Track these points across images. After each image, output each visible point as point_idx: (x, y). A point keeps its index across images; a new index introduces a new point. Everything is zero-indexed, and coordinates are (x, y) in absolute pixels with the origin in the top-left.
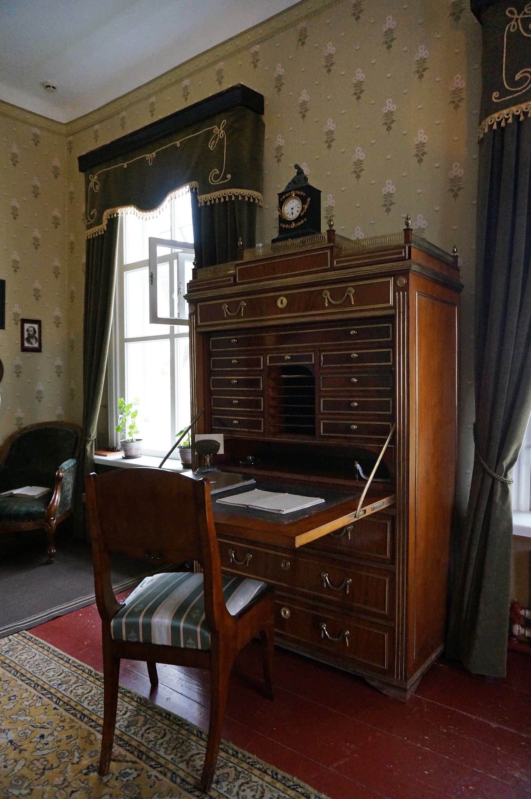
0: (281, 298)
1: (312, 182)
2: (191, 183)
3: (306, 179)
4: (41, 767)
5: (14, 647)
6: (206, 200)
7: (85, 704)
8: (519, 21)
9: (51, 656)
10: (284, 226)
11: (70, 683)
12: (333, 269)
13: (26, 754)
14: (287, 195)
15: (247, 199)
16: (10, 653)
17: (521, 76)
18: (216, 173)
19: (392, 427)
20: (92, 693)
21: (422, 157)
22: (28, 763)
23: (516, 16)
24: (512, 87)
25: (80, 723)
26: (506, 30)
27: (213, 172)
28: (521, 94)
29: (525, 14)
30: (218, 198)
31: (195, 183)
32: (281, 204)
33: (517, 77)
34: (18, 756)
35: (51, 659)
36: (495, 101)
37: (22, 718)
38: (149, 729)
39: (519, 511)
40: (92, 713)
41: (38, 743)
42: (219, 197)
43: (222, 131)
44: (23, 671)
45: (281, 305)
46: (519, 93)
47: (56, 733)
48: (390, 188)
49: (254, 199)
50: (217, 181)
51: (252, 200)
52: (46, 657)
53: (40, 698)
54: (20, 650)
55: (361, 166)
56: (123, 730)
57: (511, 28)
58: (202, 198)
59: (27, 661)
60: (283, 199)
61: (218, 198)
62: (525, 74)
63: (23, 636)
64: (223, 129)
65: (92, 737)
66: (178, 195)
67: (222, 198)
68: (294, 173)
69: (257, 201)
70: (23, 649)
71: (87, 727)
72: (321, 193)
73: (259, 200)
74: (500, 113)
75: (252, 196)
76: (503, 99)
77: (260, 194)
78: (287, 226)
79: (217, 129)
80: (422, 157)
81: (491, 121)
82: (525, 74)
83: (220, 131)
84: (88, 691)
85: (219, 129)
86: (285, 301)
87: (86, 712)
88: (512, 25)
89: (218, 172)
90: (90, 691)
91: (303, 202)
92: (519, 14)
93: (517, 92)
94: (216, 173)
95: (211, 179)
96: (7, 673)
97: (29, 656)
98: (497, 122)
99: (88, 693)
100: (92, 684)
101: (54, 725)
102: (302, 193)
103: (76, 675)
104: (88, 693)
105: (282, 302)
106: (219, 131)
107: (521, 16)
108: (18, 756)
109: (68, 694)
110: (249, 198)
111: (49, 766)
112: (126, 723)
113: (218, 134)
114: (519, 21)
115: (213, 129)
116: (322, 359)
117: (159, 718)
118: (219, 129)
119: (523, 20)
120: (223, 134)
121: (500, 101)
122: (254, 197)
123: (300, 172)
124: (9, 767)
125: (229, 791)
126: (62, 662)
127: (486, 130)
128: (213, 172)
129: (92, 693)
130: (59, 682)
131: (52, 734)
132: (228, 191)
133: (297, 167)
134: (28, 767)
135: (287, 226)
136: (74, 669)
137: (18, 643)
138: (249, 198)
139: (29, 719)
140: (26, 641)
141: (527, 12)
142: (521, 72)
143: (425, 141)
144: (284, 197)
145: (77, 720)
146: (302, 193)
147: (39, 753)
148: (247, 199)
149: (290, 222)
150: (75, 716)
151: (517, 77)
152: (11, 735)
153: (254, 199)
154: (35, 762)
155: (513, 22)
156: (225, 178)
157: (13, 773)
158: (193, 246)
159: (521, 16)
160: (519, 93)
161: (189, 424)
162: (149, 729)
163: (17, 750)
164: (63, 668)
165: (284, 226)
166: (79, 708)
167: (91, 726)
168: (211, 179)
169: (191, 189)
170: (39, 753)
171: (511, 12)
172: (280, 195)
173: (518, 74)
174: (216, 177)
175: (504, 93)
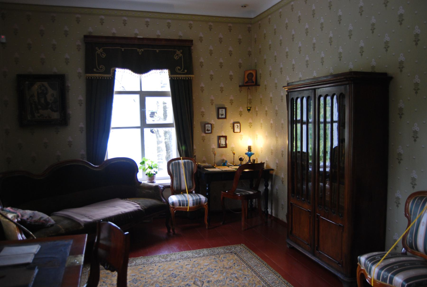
4: (243, 285)
5: (242, 251)
7: (261, 273)
9: (254, 256)
11: (276, 283)
13: (240, 281)
16: (240, 253)
19: (415, 223)
20: (264, 271)
22: (240, 283)
23: (180, 52)
25: (258, 277)
33: (100, 67)
34: (237, 281)
35: (253, 257)
37: (240, 272)
38: (279, 285)
40: (262, 276)
41: (244, 279)
44: (243, 259)
47: (250, 278)
50: (179, 71)
52: (252, 257)
53: (247, 268)
54: (278, 284)
56: (271, 283)
59: (262, 271)
63: (245, 248)
65: (260, 282)
70: (260, 266)
71: (260, 279)
84: (263, 270)
87: (261, 276)
90: (264, 270)
93: (100, 71)
95: (103, 70)
96: (238, 258)
97: (272, 278)
99: (263, 271)
100: (265, 268)
101: (249, 276)
103: (260, 264)
104: (263, 271)
108: (237, 281)
109: (256, 269)
111: (245, 285)
112: (272, 282)
117: (284, 283)
124: (234, 283)
125: (274, 285)
126: (257, 259)
128: (177, 71)
129: (264, 271)
130: (254, 265)
131: (248, 278)
134: (239, 284)
136: (260, 262)
137: (243, 250)
139: (242, 272)
140: (246, 250)
145: (257, 277)
147: (243, 282)
150: (257, 275)
151: (100, 67)
152: (236, 275)
153: (191, 78)
154: (242, 283)
156: (183, 71)
157: (235, 284)
162: (279, 285)
163: (237, 279)
164: (257, 261)
166: (259, 274)
167: (261, 279)
168: (103, 70)
170: (243, 282)
174: (179, 70)
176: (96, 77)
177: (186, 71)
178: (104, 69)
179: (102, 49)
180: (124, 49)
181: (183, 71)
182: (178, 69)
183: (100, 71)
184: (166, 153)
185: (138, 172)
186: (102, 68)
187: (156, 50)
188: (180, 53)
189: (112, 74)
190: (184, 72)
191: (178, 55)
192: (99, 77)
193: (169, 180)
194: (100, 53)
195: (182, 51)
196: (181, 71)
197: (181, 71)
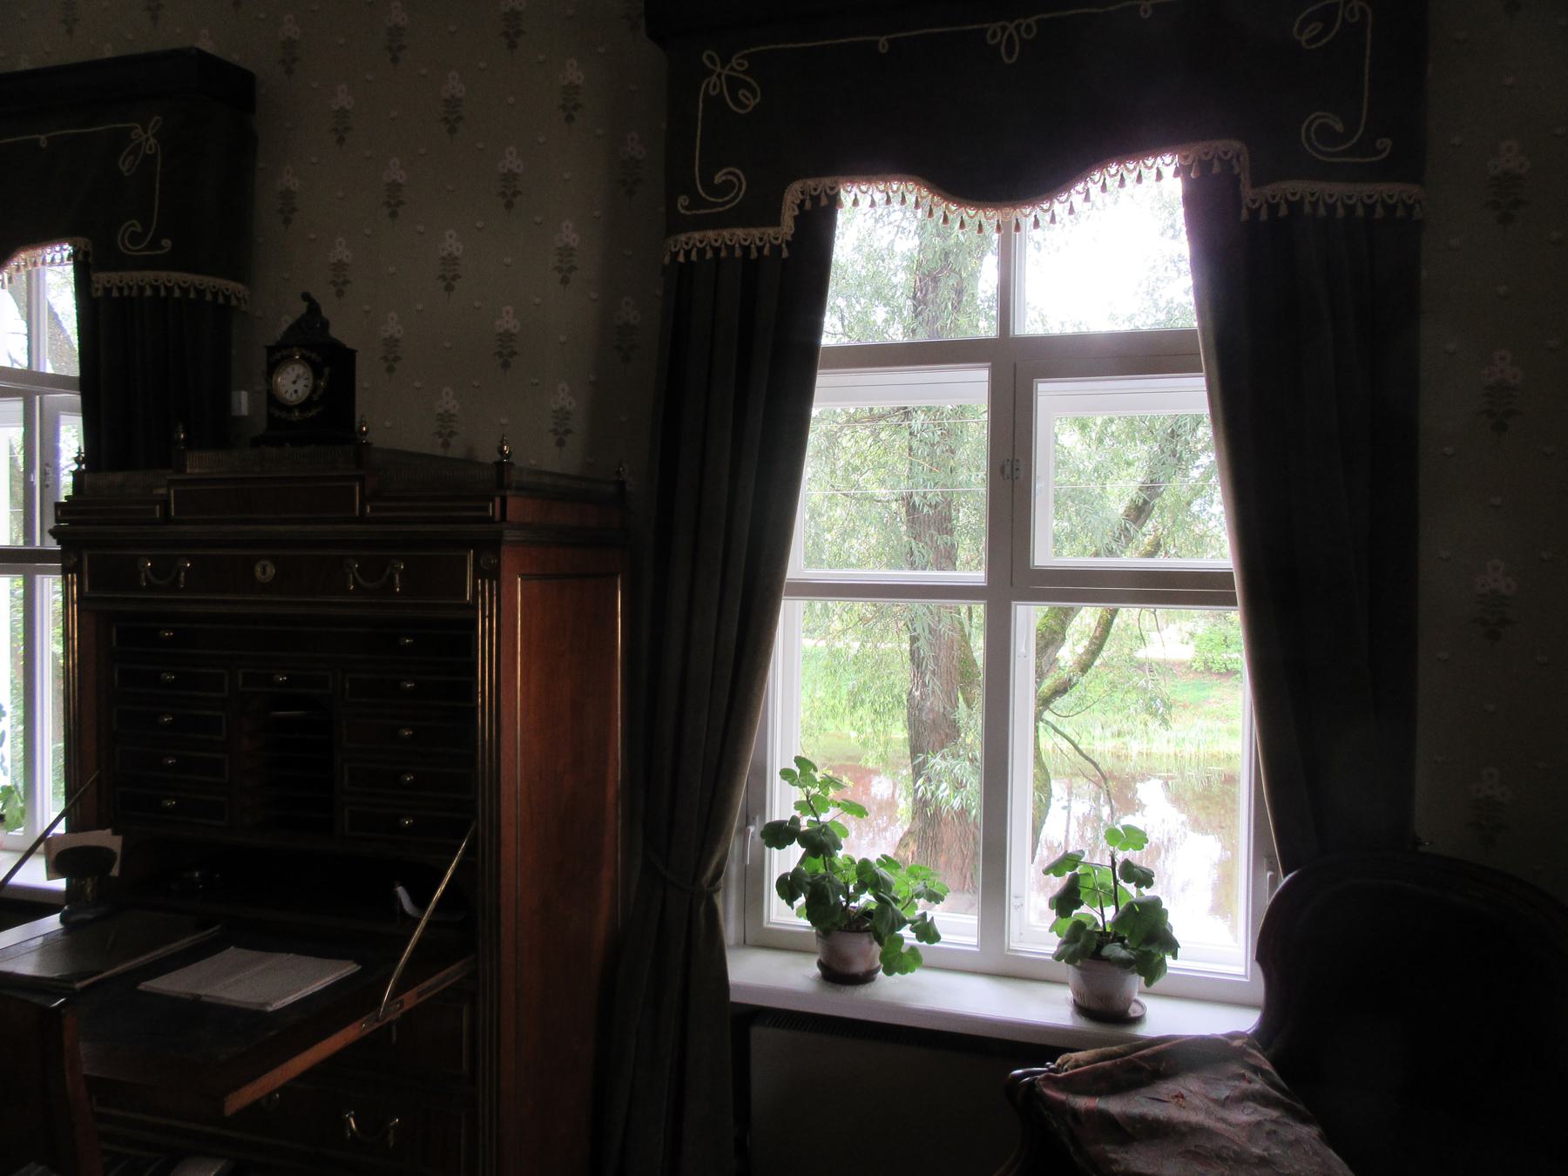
0: (263, 562)
1: (339, 332)
2: (74, 238)
3: (325, 325)
6: (108, 286)
8: (723, 78)
10: (277, 413)
12: (362, 519)
14: (285, 353)
15: (209, 297)
17: (724, 178)
18: (134, 229)
21: (510, 359)
23: (718, 69)
24: (710, 196)
26: (703, 89)
27: (129, 250)
28: (724, 211)
29: (732, 69)
30: (138, 285)
31: (82, 241)
32: (273, 368)
33: (719, 178)
36: (683, 211)
39: (731, 947)
42: (140, 283)
43: (152, 141)
45: (263, 577)
46: (721, 209)
48: (508, 321)
49: (227, 298)
51: (221, 300)
55: (457, 267)
57: (711, 88)
58: (101, 278)
60: (276, 359)
61: (138, 285)
62: (730, 177)
64: (154, 136)
66: (41, 259)
67: (148, 287)
68: (302, 307)
69: (234, 302)
72: (357, 354)
73: (238, 299)
74: (689, 234)
75: (222, 291)
76: (694, 212)
77: (240, 286)
78: (284, 415)
79: (139, 130)
80: (510, 359)
81: (675, 247)
82: (730, 177)
83: (148, 139)
85: (146, 132)
86: (271, 571)
88: (712, 82)
89: (139, 229)
91: (317, 374)
92: (723, 67)
93: (715, 205)
94: (134, 229)
98: (684, 249)
102: (314, 356)
105: (265, 571)
106: (146, 137)
107: (726, 71)
110: (215, 295)
113: (140, 144)
114: (723, 78)
115: (132, 129)
116: (347, 685)
118: (146, 132)
119: (729, 78)
120: (153, 146)
121: (688, 213)
122: (228, 293)
123: (313, 308)
127: (667, 260)
128: (129, 250)
132: (163, 275)
133: (306, 297)
135: (284, 415)
138: (215, 295)
141: (735, 66)
142: (724, 171)
143: (515, 331)
144: (278, 355)
146: (314, 356)
148: (209, 297)
149: (288, 408)
151: (719, 178)
155: (714, 78)
156: (154, 244)
158: (78, 382)
159: (726, 71)
160: (721, 209)
161: (61, 806)
165: (277, 413)
169: (74, 257)
171: (710, 58)
172: (271, 350)
173: (720, 174)
174: (135, 238)
175: (696, 202)
176: (200, 292)
177: (1385, 144)
178: (124, 245)
179: (743, 57)
180: (890, 41)
181: (154, 244)
182: (731, 181)
183: (715, 205)
184: (1148, 783)
185: (1165, 913)
186: (727, 187)
187: (38, 140)
188: (723, 67)
189: (787, 226)
190: (162, 248)
191: (734, 84)
192: (1370, 209)
193: (799, 959)
194: (137, 142)
195: (1142, 14)
196: (139, 247)
197: (139, 247)
